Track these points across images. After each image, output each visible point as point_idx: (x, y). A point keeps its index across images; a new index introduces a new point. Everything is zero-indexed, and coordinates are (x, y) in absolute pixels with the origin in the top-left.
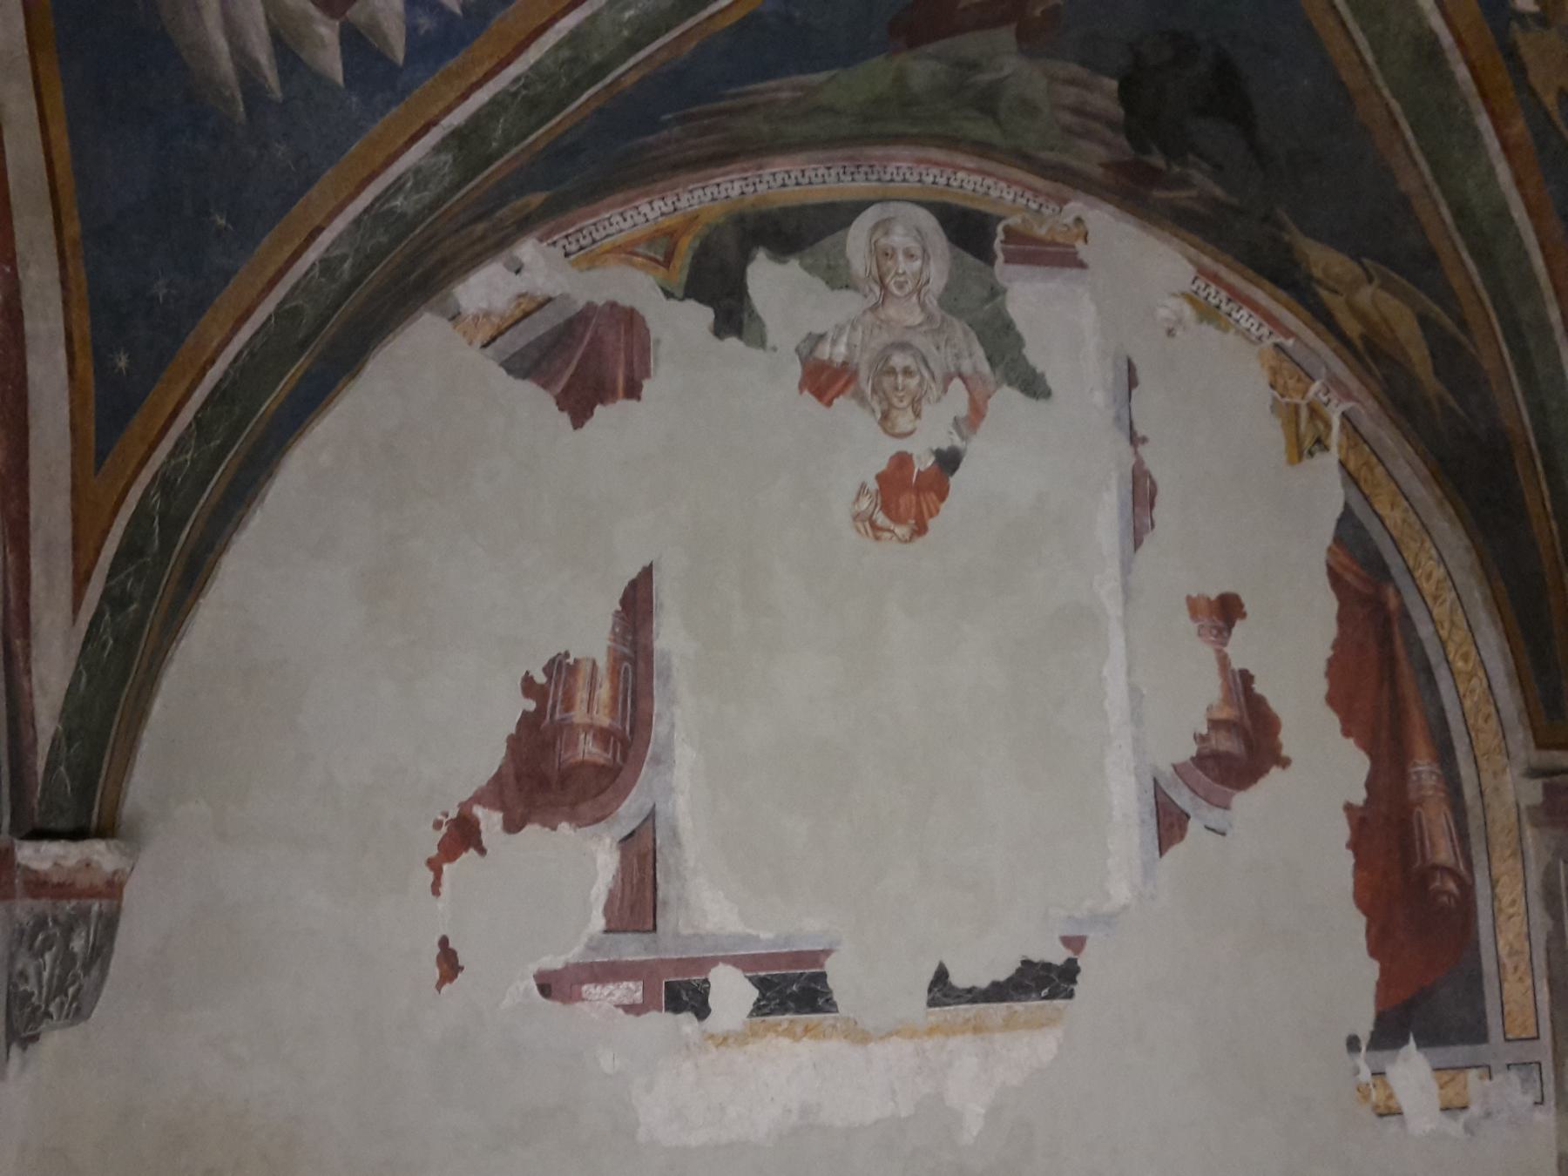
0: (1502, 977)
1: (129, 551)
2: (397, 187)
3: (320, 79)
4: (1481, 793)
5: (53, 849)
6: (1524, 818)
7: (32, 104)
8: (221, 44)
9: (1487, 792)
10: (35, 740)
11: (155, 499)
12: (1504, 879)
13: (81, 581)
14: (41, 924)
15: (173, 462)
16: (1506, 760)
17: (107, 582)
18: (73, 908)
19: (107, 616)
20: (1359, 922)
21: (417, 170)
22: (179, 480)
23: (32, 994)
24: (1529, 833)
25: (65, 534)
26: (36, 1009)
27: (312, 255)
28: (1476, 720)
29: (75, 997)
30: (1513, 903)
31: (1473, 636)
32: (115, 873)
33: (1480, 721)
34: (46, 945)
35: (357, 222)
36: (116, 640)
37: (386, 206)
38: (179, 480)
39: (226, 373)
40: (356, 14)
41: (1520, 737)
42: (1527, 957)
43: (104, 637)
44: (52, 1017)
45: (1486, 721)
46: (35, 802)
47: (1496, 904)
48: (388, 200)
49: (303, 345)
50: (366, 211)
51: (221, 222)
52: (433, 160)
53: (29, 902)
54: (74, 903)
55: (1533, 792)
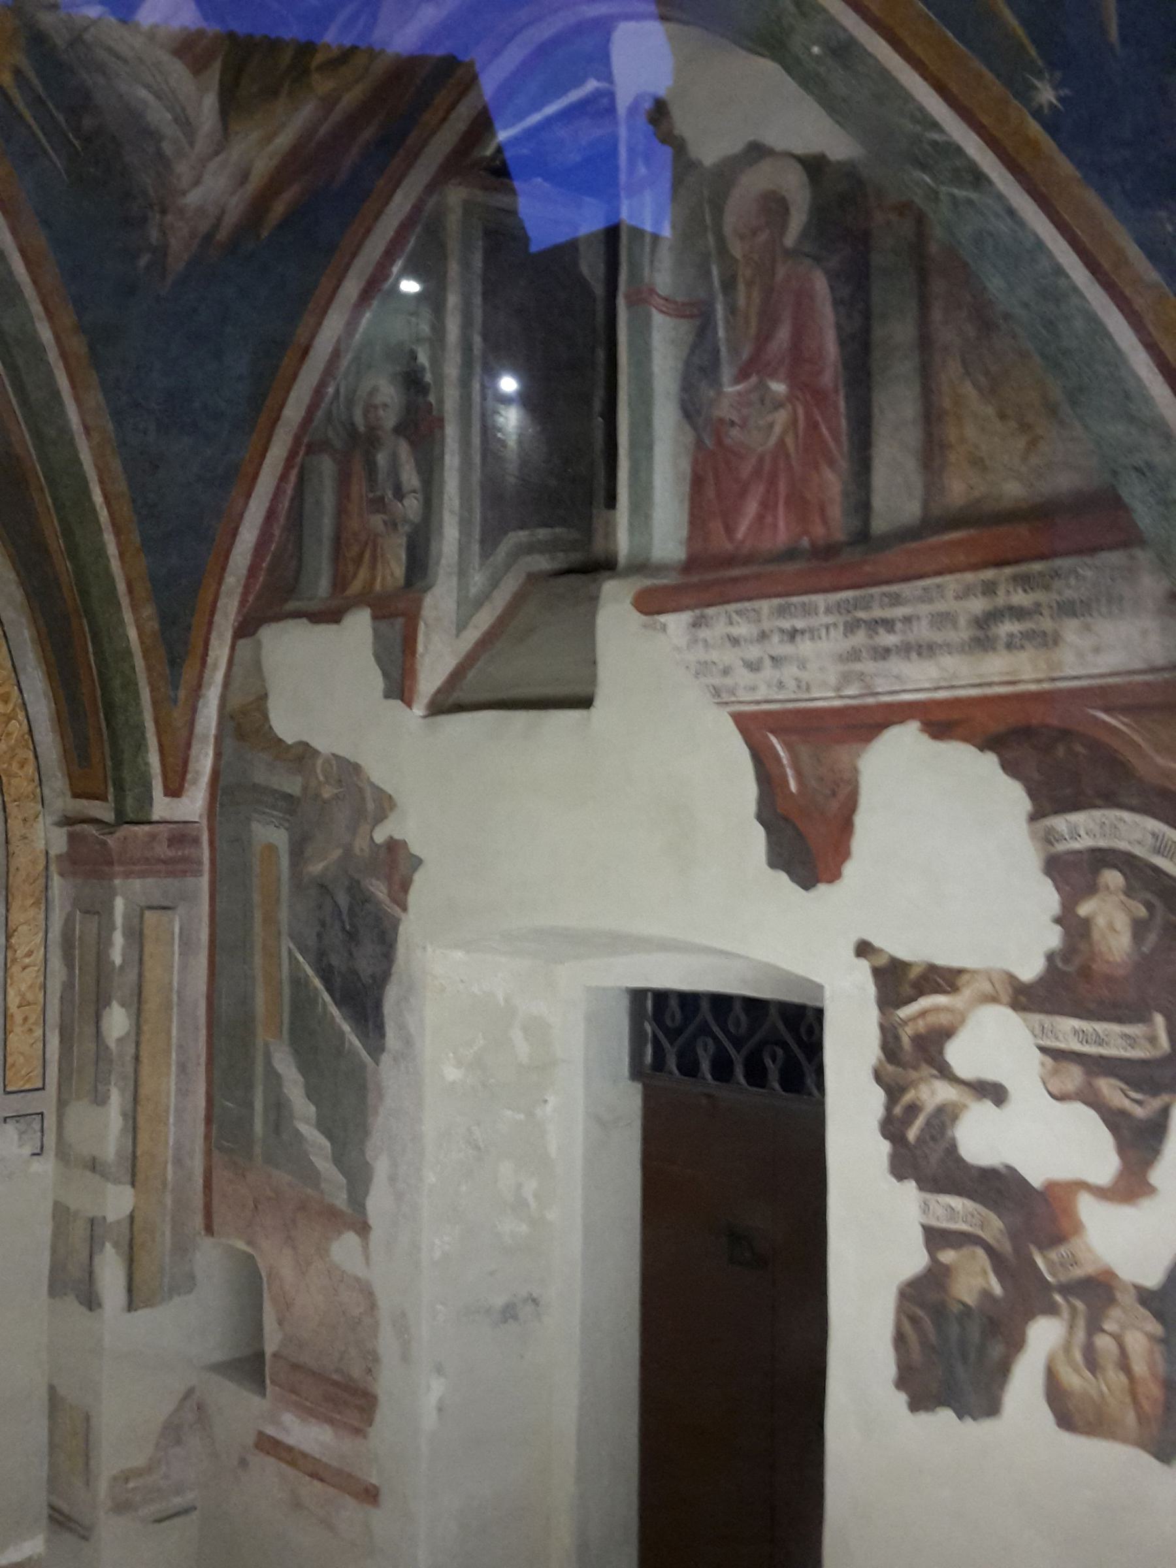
0: (8, 1027)
4: (7, 842)
6: (53, 868)
9: (14, 840)
12: (23, 929)
16: (40, 806)
20: (783, 877)
24: (56, 881)
28: (10, 765)
30: (29, 954)
31: (16, 675)
33: (15, 767)
41: (57, 782)
42: (39, 1008)
45: (22, 766)
47: (10, 954)
55: (59, 841)
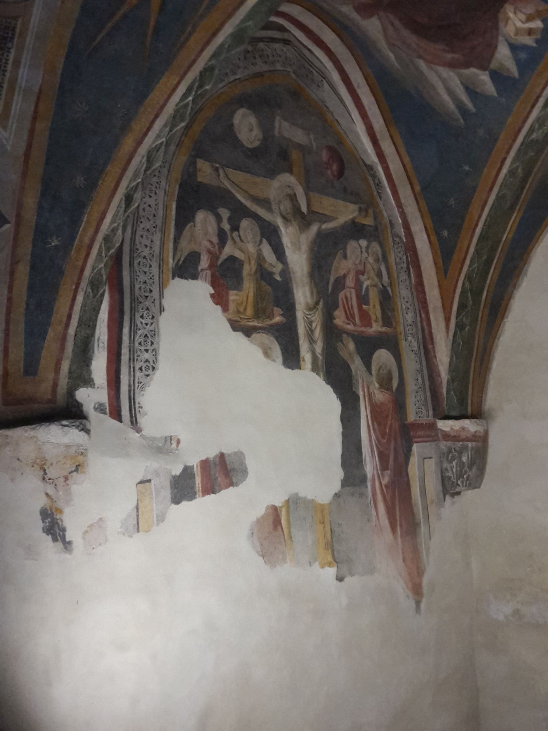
1: (462, 307)
2: (531, 130)
3: (488, 98)
5: (450, 422)
7: (393, 148)
8: (446, 98)
10: (442, 382)
11: (467, 285)
13: (447, 320)
14: (450, 451)
15: (471, 269)
17: (457, 319)
18: (461, 445)
19: (459, 333)
21: (538, 119)
22: (474, 275)
23: (450, 477)
25: (439, 304)
26: (453, 482)
27: (504, 171)
29: (467, 479)
32: (476, 432)
34: (453, 459)
35: (519, 150)
36: (463, 342)
37: (530, 139)
38: (474, 275)
39: (483, 229)
40: (494, 65)
43: (459, 341)
44: (460, 486)
46: (445, 406)
48: (530, 136)
49: (512, 208)
50: (522, 144)
51: (467, 168)
52: (543, 113)
53: (445, 442)
54: (461, 443)
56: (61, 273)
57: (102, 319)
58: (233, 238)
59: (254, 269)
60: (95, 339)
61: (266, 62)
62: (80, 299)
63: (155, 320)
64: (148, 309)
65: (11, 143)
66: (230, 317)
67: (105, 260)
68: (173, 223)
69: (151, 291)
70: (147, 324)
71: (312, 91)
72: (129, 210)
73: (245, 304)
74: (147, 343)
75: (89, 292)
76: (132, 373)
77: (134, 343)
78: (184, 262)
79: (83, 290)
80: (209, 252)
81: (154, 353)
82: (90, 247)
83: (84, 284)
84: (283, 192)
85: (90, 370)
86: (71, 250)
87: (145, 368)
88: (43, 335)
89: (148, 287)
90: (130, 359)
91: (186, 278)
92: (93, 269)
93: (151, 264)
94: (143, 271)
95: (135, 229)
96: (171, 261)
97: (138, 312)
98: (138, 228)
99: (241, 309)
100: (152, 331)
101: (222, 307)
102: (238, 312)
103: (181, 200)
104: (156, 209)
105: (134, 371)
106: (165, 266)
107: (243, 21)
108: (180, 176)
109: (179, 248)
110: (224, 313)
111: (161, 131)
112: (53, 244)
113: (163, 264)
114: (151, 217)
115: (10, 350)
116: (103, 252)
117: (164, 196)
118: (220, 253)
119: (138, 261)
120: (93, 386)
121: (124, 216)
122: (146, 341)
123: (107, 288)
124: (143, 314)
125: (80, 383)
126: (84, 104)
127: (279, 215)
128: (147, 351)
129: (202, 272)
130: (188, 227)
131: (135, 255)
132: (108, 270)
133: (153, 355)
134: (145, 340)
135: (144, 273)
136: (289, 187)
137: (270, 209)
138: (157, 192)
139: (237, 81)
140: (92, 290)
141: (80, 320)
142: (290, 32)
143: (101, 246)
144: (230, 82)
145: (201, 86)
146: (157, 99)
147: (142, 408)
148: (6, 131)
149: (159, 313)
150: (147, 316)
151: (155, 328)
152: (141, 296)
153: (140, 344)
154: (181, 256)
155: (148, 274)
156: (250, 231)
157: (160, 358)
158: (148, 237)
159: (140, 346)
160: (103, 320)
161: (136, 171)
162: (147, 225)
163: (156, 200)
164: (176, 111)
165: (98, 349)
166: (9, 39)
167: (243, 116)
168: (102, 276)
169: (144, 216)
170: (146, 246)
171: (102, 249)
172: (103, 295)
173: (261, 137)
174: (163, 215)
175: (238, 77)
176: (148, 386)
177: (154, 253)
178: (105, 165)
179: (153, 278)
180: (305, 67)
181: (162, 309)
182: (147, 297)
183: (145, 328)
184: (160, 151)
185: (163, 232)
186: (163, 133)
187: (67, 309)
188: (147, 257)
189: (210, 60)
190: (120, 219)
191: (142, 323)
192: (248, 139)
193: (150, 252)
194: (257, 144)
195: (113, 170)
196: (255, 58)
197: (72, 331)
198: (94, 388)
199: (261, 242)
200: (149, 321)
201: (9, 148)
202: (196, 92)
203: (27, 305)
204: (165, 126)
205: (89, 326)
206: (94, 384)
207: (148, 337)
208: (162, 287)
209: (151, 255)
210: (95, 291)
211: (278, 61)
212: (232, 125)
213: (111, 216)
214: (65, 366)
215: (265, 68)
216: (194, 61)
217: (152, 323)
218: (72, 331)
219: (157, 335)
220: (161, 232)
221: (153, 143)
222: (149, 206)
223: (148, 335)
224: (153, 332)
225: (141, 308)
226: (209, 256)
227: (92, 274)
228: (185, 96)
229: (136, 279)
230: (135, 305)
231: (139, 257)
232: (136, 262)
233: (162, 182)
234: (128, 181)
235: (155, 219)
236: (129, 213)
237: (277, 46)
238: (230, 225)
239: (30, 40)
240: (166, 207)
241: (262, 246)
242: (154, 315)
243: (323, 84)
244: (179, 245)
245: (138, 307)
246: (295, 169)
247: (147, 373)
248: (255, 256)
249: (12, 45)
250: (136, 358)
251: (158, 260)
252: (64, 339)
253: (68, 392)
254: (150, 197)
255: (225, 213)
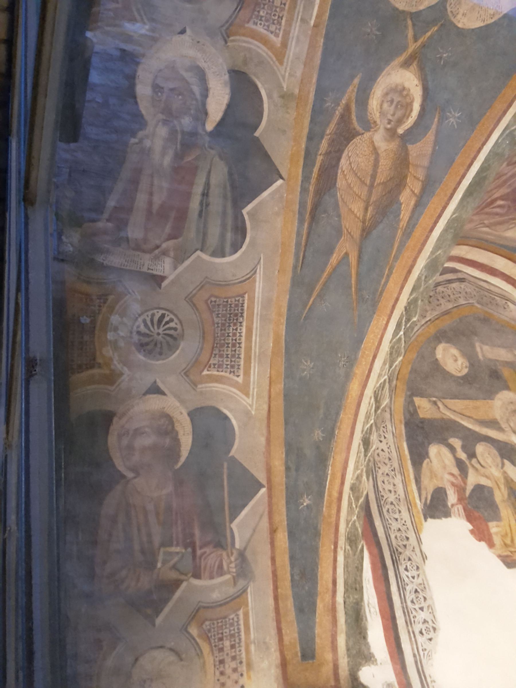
56: (317, 534)
57: (367, 580)
58: (473, 466)
59: (506, 496)
60: (364, 604)
61: (449, 301)
62: (341, 558)
63: (420, 572)
64: (410, 559)
65: (254, 407)
66: (499, 552)
67: (356, 512)
68: (409, 462)
69: (408, 538)
70: (413, 578)
71: (501, 314)
72: (368, 454)
73: (509, 535)
74: (419, 600)
75: (348, 550)
76: (413, 639)
77: (406, 602)
78: (431, 500)
79: (341, 548)
80: (453, 484)
81: (430, 610)
82: (340, 499)
83: (342, 541)
84: (507, 409)
85: (368, 643)
86: (323, 507)
87: (425, 630)
88: (313, 606)
89: (404, 535)
90: (406, 622)
91: (439, 518)
92: (347, 524)
93: (400, 509)
94: (394, 518)
95: (375, 476)
96: (418, 501)
97: (401, 564)
98: (377, 474)
99: (508, 541)
100: (421, 584)
101: (486, 542)
102: (506, 545)
103: (411, 438)
104: (390, 452)
105: (415, 636)
106: (413, 508)
107: (432, 253)
108: (403, 417)
109: (422, 487)
110: (491, 550)
111: (382, 369)
112: (305, 504)
113: (412, 507)
114: (387, 461)
115: (283, 632)
116: (353, 503)
117: (393, 438)
118: (465, 483)
119: (386, 509)
120: (375, 663)
121: (365, 461)
122: (418, 597)
123: (363, 542)
124: (406, 566)
125: (361, 661)
126: (309, 361)
127: (512, 432)
128: (422, 609)
129: (453, 508)
130: (425, 464)
131: (382, 503)
132: (361, 523)
133: (430, 613)
134: (417, 596)
135: (395, 520)
136: (512, 403)
137: (500, 429)
138: (386, 436)
139: (429, 323)
140: (351, 547)
141: (346, 583)
142: (463, 272)
143: (349, 497)
144: (423, 325)
145: (408, 320)
146: (372, 341)
147: (434, 682)
148: (248, 397)
149: (423, 562)
150: (411, 567)
151: (423, 580)
152: (399, 546)
153: (412, 602)
154: (427, 494)
155: (399, 520)
156: (488, 455)
157: (438, 615)
158: (390, 481)
159: (413, 604)
160: (368, 581)
161: (367, 413)
162: (386, 469)
163: (387, 443)
164: (392, 348)
165: (371, 616)
166: (240, 315)
167: (444, 350)
168: (357, 529)
169: (380, 462)
170: (390, 491)
171: (351, 499)
172: (362, 551)
173: (468, 364)
174: (398, 457)
175: (428, 319)
176: (435, 653)
177: (400, 497)
178: (338, 414)
179: (405, 524)
180: (486, 296)
181: (424, 558)
182: (405, 546)
183: (412, 582)
184: (385, 389)
185: (403, 473)
186: (384, 372)
187: (331, 572)
188: (394, 503)
189: (411, 294)
190: (362, 466)
191: (408, 577)
192: (457, 370)
193: (396, 496)
194: (465, 371)
195: (346, 417)
196: (438, 300)
197: (340, 598)
198: (377, 664)
199: (503, 464)
200: (415, 573)
201: (253, 413)
202: (406, 325)
203: (292, 576)
204: (384, 363)
205: (356, 589)
206: (376, 660)
207: (418, 592)
208: (417, 532)
209: (398, 500)
210: (354, 548)
211: (460, 297)
212: (437, 360)
213: (353, 464)
214: (342, 641)
215: (450, 306)
216: (397, 299)
217: (418, 575)
218: (340, 598)
219: (427, 589)
220: (400, 474)
221: (377, 382)
222: (382, 450)
223: (419, 590)
224: (423, 586)
225: (403, 560)
226: (455, 490)
227: (348, 530)
228: (396, 332)
229: (390, 528)
230: (396, 558)
231: (387, 504)
232: (385, 510)
233: (387, 426)
234: (362, 424)
235: (391, 462)
236: (369, 457)
237: (454, 285)
238: (466, 453)
239: (257, 309)
240: (399, 449)
241: (505, 468)
242: (418, 565)
243: (508, 306)
244: (422, 483)
245: (399, 559)
246: (511, 385)
247: (429, 637)
248: (502, 480)
249: (243, 319)
250: (412, 620)
251: (406, 503)
252: (333, 610)
253: (350, 674)
254: (381, 441)
255: (457, 443)
